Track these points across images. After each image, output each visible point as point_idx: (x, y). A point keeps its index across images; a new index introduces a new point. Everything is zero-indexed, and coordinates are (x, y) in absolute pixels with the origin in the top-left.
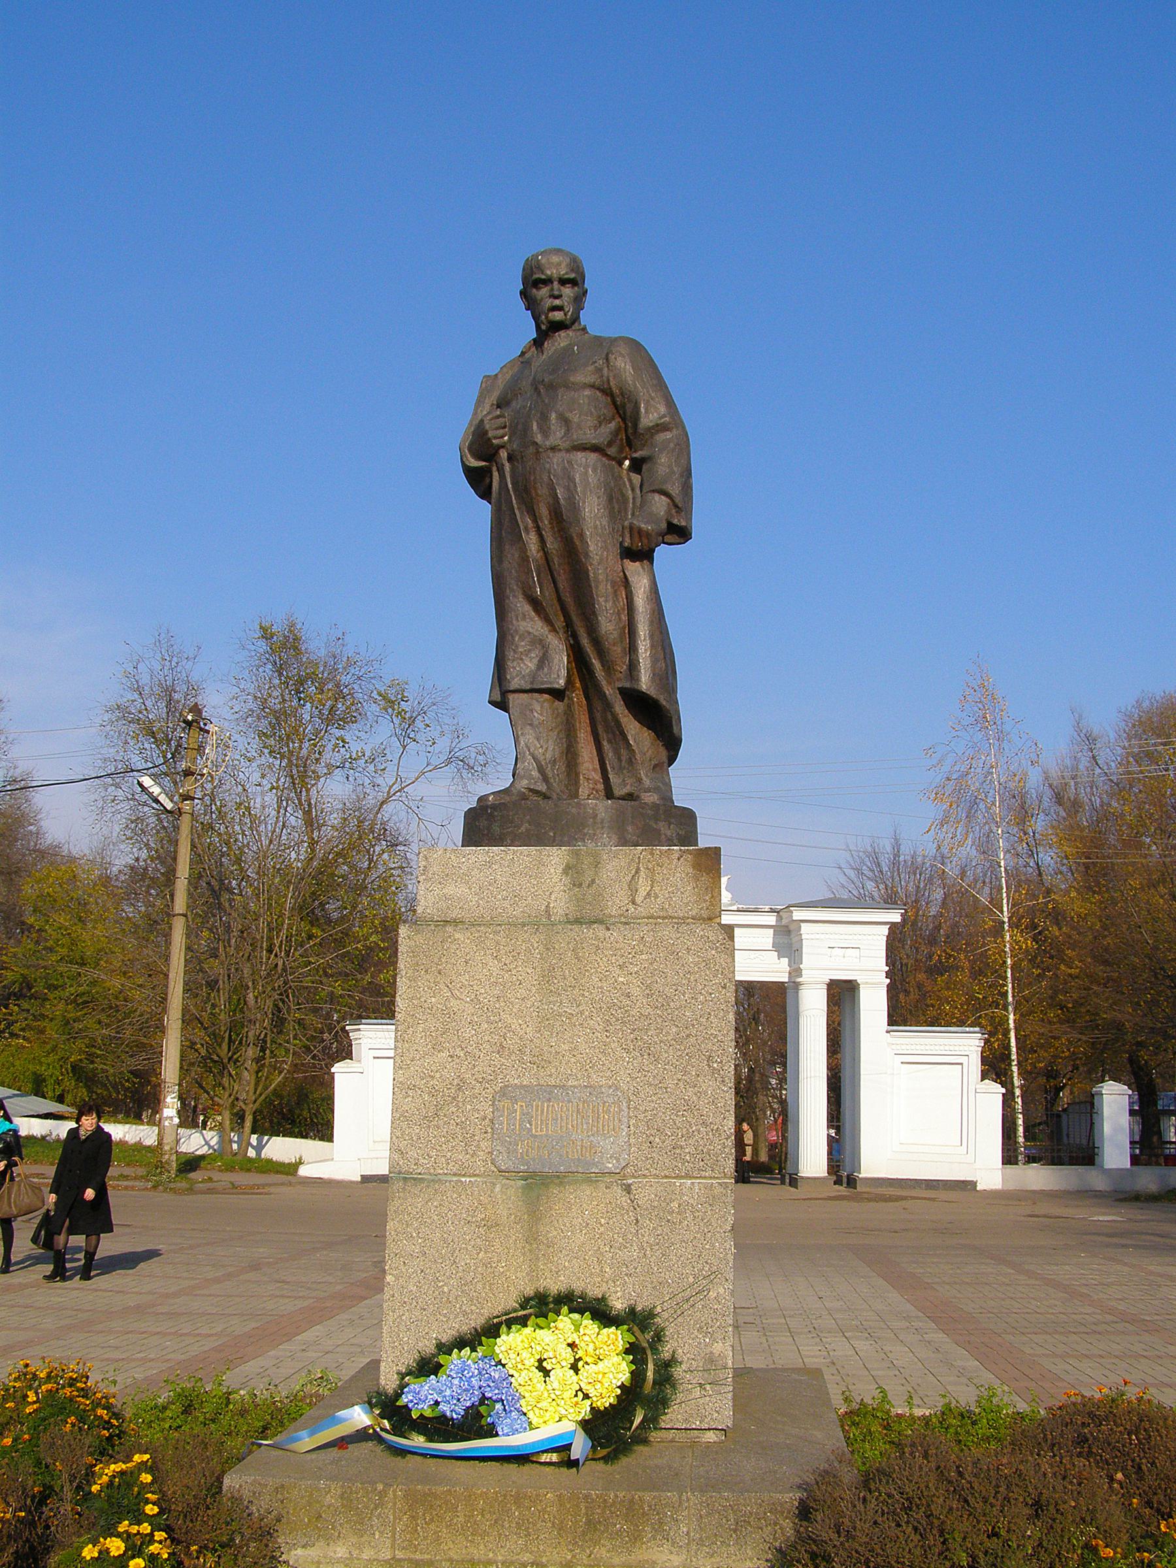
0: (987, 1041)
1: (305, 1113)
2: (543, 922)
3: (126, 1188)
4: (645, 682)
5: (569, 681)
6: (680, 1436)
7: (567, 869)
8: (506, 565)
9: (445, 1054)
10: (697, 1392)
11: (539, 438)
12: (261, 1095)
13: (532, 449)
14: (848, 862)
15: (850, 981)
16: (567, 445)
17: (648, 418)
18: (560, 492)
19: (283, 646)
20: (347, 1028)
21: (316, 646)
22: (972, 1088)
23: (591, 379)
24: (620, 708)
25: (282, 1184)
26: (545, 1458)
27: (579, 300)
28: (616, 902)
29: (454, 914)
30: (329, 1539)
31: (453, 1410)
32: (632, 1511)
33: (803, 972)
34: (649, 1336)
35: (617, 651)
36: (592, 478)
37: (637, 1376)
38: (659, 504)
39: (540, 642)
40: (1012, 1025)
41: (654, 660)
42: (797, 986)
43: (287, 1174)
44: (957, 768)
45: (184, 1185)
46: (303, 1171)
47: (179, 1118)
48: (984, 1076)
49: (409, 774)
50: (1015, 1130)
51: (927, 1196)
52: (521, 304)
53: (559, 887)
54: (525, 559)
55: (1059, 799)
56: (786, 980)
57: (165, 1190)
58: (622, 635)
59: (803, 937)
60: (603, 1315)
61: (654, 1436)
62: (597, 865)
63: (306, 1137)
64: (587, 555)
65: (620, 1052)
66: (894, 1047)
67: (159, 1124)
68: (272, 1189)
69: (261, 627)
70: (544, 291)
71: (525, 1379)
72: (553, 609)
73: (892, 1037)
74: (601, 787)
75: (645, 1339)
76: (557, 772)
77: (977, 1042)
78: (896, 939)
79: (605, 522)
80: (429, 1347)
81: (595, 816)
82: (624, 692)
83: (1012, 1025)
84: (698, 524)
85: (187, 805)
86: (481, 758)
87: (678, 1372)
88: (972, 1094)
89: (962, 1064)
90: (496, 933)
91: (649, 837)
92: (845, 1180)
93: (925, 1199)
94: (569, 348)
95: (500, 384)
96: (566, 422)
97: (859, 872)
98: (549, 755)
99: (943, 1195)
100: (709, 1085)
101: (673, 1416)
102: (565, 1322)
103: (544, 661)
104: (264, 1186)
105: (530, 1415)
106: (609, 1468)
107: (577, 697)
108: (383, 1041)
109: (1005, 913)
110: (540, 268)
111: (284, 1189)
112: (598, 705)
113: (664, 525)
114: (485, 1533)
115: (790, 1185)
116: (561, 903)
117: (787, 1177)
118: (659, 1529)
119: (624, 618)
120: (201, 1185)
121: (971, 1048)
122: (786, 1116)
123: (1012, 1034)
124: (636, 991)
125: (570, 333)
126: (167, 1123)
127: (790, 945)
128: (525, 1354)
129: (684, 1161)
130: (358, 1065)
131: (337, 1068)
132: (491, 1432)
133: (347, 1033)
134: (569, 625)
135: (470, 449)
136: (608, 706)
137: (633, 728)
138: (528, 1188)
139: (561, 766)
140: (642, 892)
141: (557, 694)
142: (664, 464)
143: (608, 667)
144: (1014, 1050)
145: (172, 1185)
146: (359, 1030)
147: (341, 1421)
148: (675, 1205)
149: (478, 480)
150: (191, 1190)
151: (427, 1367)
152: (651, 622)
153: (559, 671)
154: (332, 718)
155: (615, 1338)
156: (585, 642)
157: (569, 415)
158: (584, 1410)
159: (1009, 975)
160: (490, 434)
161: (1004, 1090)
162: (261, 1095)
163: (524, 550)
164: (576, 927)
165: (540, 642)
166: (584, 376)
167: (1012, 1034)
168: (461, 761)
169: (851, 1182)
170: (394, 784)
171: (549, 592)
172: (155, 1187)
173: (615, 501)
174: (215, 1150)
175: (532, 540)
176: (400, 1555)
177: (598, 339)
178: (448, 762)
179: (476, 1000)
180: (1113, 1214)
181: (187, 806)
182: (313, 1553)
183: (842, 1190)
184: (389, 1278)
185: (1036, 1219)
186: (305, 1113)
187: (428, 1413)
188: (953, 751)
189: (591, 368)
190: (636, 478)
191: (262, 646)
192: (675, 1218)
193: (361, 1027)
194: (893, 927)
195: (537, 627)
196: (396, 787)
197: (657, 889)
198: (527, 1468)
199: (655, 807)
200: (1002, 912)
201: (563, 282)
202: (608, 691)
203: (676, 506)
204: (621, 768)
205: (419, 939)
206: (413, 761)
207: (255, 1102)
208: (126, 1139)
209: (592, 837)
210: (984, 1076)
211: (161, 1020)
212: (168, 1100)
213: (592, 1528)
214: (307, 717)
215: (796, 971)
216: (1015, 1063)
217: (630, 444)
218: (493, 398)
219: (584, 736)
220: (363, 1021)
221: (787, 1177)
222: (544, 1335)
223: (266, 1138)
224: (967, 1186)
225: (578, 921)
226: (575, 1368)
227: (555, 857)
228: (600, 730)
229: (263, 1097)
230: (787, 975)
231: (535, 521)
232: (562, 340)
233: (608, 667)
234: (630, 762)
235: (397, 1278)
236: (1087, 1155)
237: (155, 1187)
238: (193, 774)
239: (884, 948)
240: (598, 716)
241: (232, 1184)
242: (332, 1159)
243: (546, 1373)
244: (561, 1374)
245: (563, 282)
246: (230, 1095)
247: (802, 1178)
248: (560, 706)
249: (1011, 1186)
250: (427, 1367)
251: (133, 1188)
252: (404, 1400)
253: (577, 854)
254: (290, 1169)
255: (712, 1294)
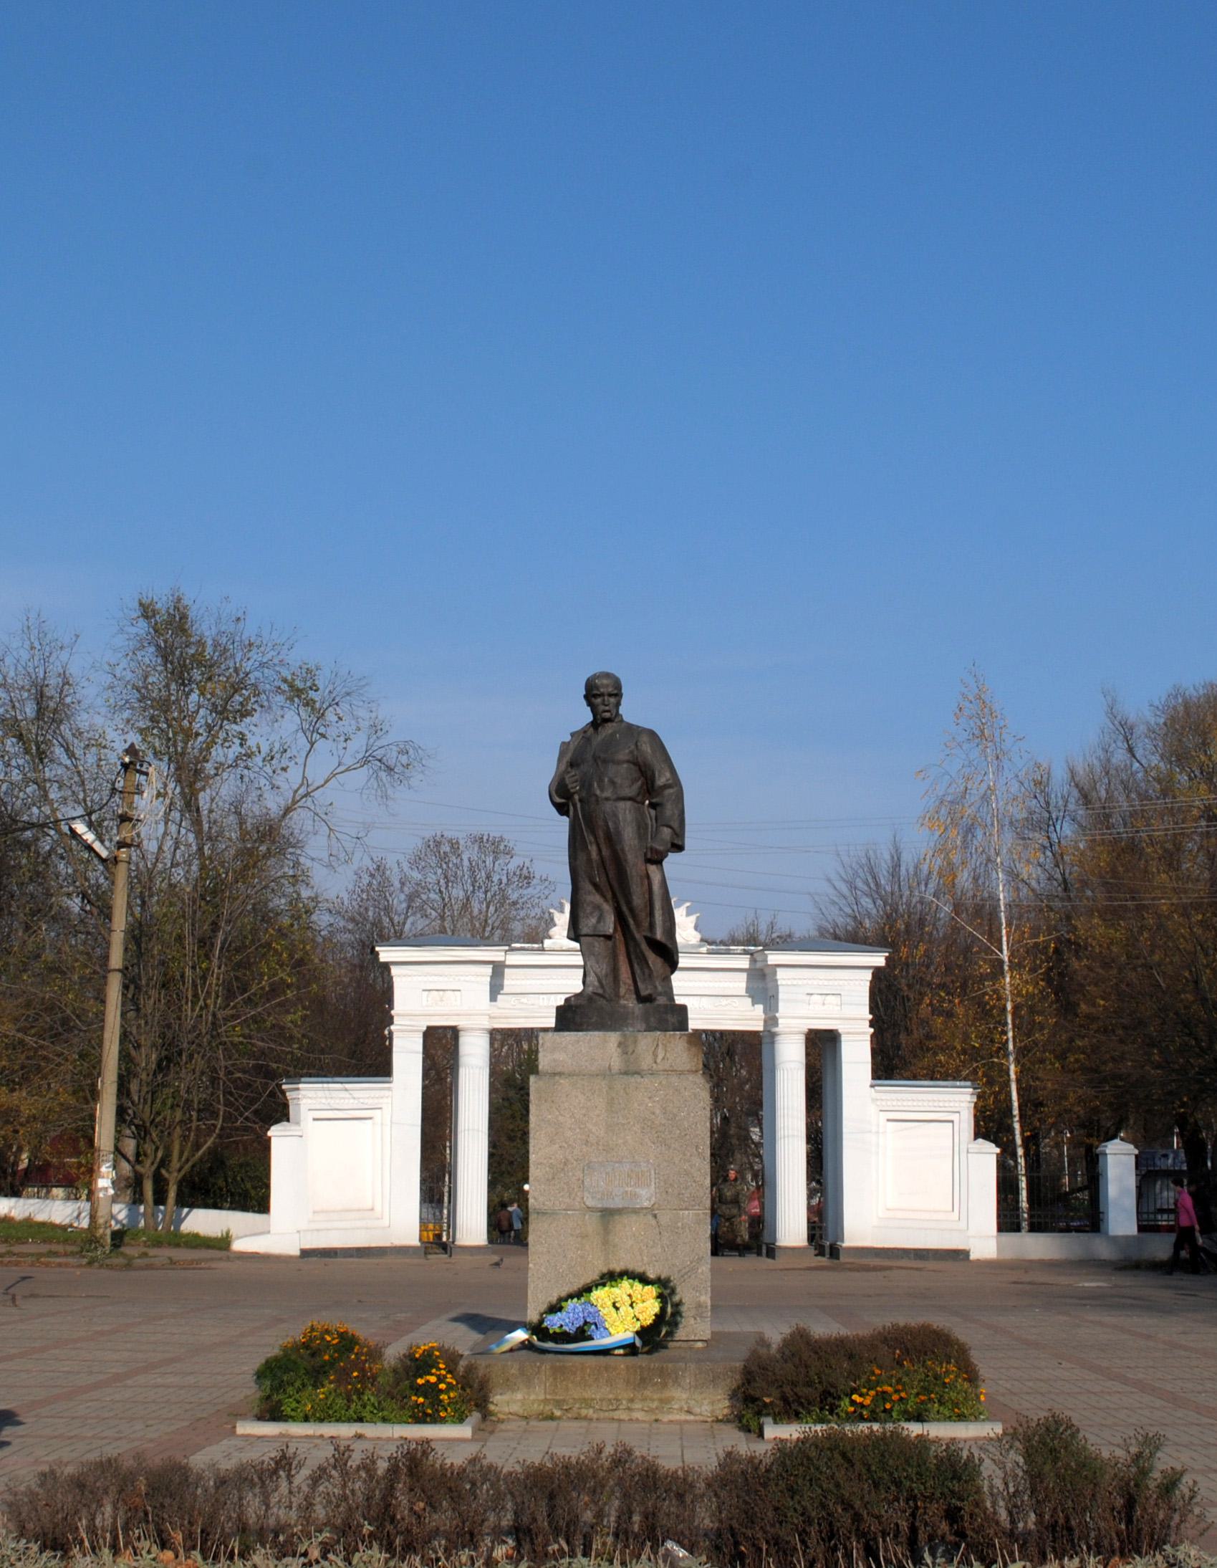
0: (979, 1097)
1: (221, 1183)
2: (606, 1074)
3: (60, 1265)
4: (659, 935)
5: (615, 929)
6: (684, 1345)
7: (620, 1045)
8: (578, 862)
9: (557, 1146)
10: (692, 1321)
11: (598, 792)
12: (188, 1160)
13: (593, 799)
14: (838, 873)
15: (831, 1031)
16: (614, 797)
17: (661, 781)
18: (610, 824)
19: (169, 623)
20: (284, 1087)
21: (205, 628)
22: (964, 1147)
23: (626, 758)
24: (644, 946)
25: (221, 1259)
26: (617, 1352)
27: (618, 704)
28: (646, 1063)
29: (558, 1070)
30: (513, 1391)
31: (570, 1329)
32: (662, 1373)
33: (780, 1021)
34: (668, 1291)
35: (643, 916)
36: (629, 817)
37: (663, 1309)
38: (666, 832)
39: (598, 907)
40: (1013, 1076)
41: (664, 922)
42: (773, 1036)
43: (220, 1249)
44: (951, 791)
45: (121, 1261)
46: (238, 1246)
47: (114, 1188)
48: (978, 1135)
49: (315, 775)
50: (1016, 1191)
51: (915, 1266)
52: (584, 702)
53: (616, 1055)
54: (589, 860)
55: (1086, 798)
56: (761, 1029)
57: (101, 1266)
58: (646, 907)
59: (779, 983)
60: (644, 1280)
61: (671, 1345)
62: (635, 1042)
63: (221, 1208)
64: (626, 860)
65: (650, 1144)
66: (878, 1103)
67: (90, 1196)
68: (214, 1265)
69: (141, 604)
70: (599, 700)
71: (606, 1311)
72: (606, 888)
73: (876, 1092)
74: (632, 988)
75: (667, 1292)
76: (608, 982)
77: (968, 1098)
78: (881, 982)
79: (636, 842)
80: (554, 1299)
81: (633, 1013)
82: (646, 938)
83: (1013, 1076)
84: (688, 842)
85: (124, 853)
86: (404, 759)
87: (683, 1309)
88: (964, 1155)
89: (952, 1122)
90: (583, 1079)
91: (663, 1026)
92: (827, 1251)
93: (912, 1268)
94: (613, 735)
95: (572, 747)
96: (612, 782)
97: (853, 887)
98: (604, 972)
99: (931, 1265)
100: (697, 1161)
101: (681, 1334)
102: (625, 1283)
103: (600, 919)
104: (207, 1260)
105: (610, 1329)
106: (649, 1357)
107: (619, 936)
108: (324, 1101)
109: (1005, 952)
110: (597, 688)
111: (222, 1265)
112: (631, 944)
113: (669, 845)
114: (590, 1386)
115: (768, 1256)
116: (616, 1063)
117: (764, 1248)
118: (676, 1382)
119: (647, 896)
120: (139, 1261)
121: (963, 1105)
122: (764, 1183)
123: (1014, 1087)
124: (658, 1112)
125: (614, 724)
126: (101, 1195)
127: (765, 990)
128: (606, 1300)
129: (684, 1201)
130: (297, 1128)
131: (275, 1132)
132: (591, 1338)
133: (283, 1093)
134: (614, 896)
135: (557, 792)
136: (637, 945)
137: (652, 958)
138: (603, 1217)
139: (611, 979)
140: (660, 1057)
141: (608, 937)
142: (669, 810)
143: (638, 924)
144: (1016, 1104)
145: (108, 1261)
146: (298, 1089)
147: (508, 1341)
148: (680, 1224)
149: (562, 809)
150: (129, 1266)
151: (555, 1308)
152: (662, 900)
153: (609, 925)
154: (222, 712)
155: (651, 1291)
156: (624, 908)
157: (616, 780)
158: (638, 1326)
159: (1009, 1021)
160: (570, 786)
161: (998, 1150)
162: (188, 1160)
163: (589, 854)
164: (625, 1077)
165: (598, 907)
166: (623, 755)
167: (1014, 1087)
168: (380, 761)
169: (834, 1252)
170: (298, 789)
171: (604, 878)
172: (90, 1263)
173: (641, 828)
174: (123, 1225)
175: (593, 849)
176: (548, 1397)
177: (630, 727)
178: (365, 761)
179: (573, 1116)
180: (1098, 1281)
181: (123, 855)
182: (505, 1397)
183: (824, 1261)
184: (531, 1265)
185: (1020, 1286)
186: (221, 1183)
187: (558, 1331)
188: (947, 773)
189: (627, 751)
190: (653, 812)
191: (142, 627)
192: (680, 1231)
193: (301, 1086)
194: (877, 972)
195: (597, 899)
196: (302, 791)
197: (668, 1055)
198: (608, 1357)
199: (666, 1006)
200: (1001, 951)
201: (610, 695)
202: (638, 936)
203: (676, 834)
204: (645, 980)
205: (541, 1083)
206: (322, 762)
207: (179, 1170)
208: (12, 1214)
209: (632, 1025)
210: (978, 1135)
211: (94, 1085)
212: (104, 1169)
213: (644, 1382)
214: (192, 707)
215: (771, 1020)
216: (1017, 1119)
217: (649, 792)
218: (567, 758)
219: (623, 960)
220: (303, 1079)
221: (764, 1248)
222: (616, 1290)
223: (186, 1210)
224: (959, 1255)
225: (626, 1073)
226: (631, 1305)
227: (613, 1038)
228: (633, 957)
229: (190, 1164)
230: (762, 1023)
231: (596, 838)
232: (609, 729)
233: (638, 924)
234: (650, 975)
235: (535, 1265)
236: (1093, 1220)
237: (90, 1263)
238: (130, 820)
239: (868, 994)
240: (632, 949)
241: (170, 1258)
242: (269, 1232)
243: (617, 1309)
244: (624, 1309)
245: (610, 695)
246: (153, 1163)
247: (780, 1248)
248: (610, 943)
249: (1009, 1255)
250: (555, 1308)
251: (66, 1265)
252: (545, 1324)
253: (625, 1036)
254: (223, 1243)
255: (700, 1271)
